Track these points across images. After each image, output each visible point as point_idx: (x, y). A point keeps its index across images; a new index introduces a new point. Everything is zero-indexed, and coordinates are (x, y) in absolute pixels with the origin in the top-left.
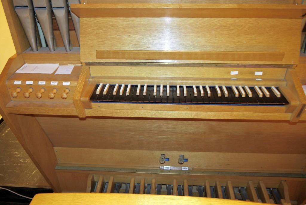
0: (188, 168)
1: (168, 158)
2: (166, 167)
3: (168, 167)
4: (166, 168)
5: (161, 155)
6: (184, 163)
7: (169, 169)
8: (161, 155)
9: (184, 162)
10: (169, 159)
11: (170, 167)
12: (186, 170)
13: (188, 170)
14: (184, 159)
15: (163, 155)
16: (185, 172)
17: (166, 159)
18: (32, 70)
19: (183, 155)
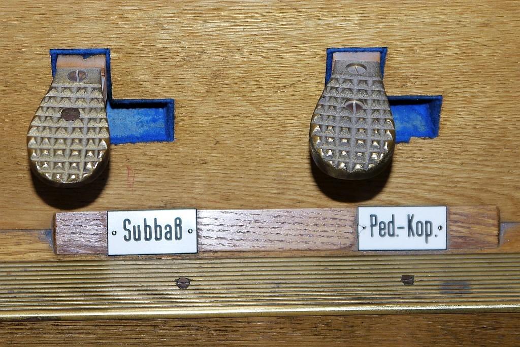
0: (437, 215)
1: (159, 93)
2: (137, 218)
3: (166, 217)
4: (134, 235)
5: (55, 55)
6: (400, 148)
7: (187, 245)
8: (55, 55)
9: (398, 138)
10: (166, 106)
11: (188, 217)
12: (417, 243)
13: (438, 242)
14: (394, 102)
15: (78, 63)
16: (408, 280)
17: (130, 120)
18: (304, 202)
19: (383, 52)
